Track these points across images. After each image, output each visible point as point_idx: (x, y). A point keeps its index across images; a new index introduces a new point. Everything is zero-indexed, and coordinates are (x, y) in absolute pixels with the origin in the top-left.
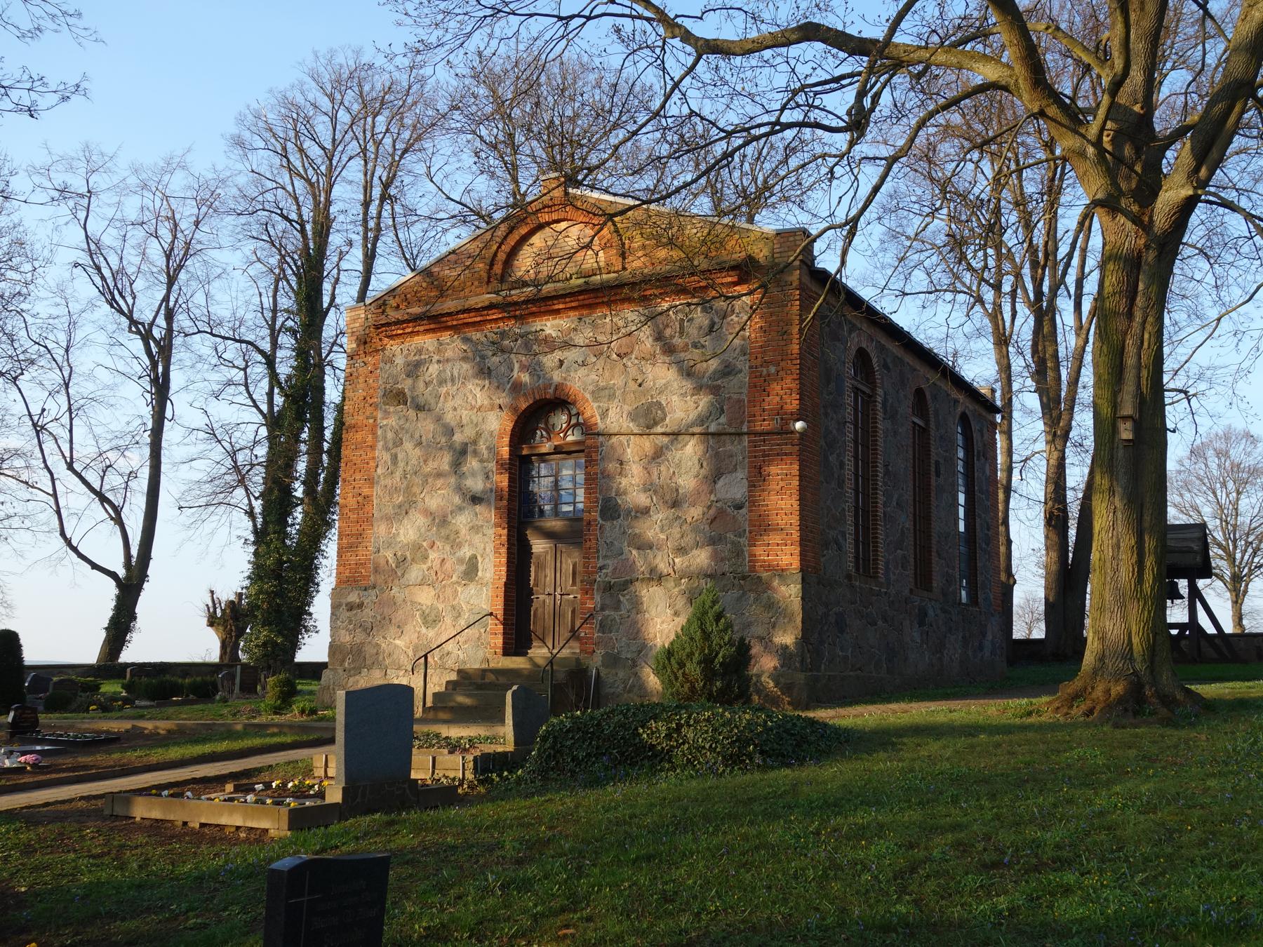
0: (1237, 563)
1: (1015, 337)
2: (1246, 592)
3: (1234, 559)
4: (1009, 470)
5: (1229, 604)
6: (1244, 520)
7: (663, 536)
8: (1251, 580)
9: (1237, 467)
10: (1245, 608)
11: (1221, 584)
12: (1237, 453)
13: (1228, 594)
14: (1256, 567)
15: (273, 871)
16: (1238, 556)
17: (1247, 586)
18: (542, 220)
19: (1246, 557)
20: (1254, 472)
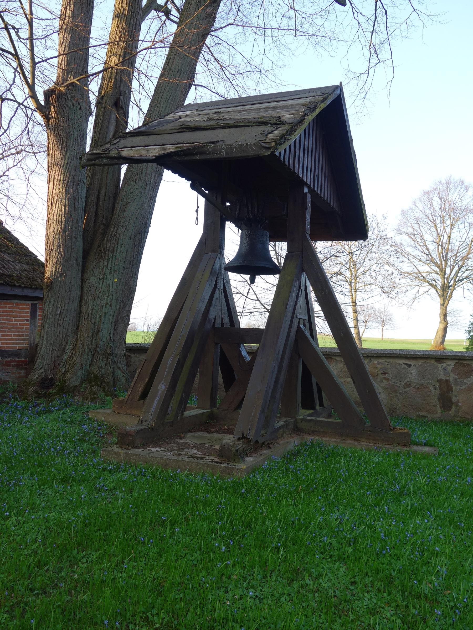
0: (446, 276)
1: (274, 138)
2: (451, 297)
3: (445, 273)
4: (357, 327)
5: (438, 306)
6: (455, 245)
7: (78, 364)
8: (455, 289)
9: (453, 209)
10: (449, 308)
11: (435, 291)
12: (453, 196)
13: (438, 299)
14: (458, 281)
15: (313, 410)
16: (448, 271)
17: (452, 293)
18: (222, 288)
19: (454, 273)
20: (466, 211)
